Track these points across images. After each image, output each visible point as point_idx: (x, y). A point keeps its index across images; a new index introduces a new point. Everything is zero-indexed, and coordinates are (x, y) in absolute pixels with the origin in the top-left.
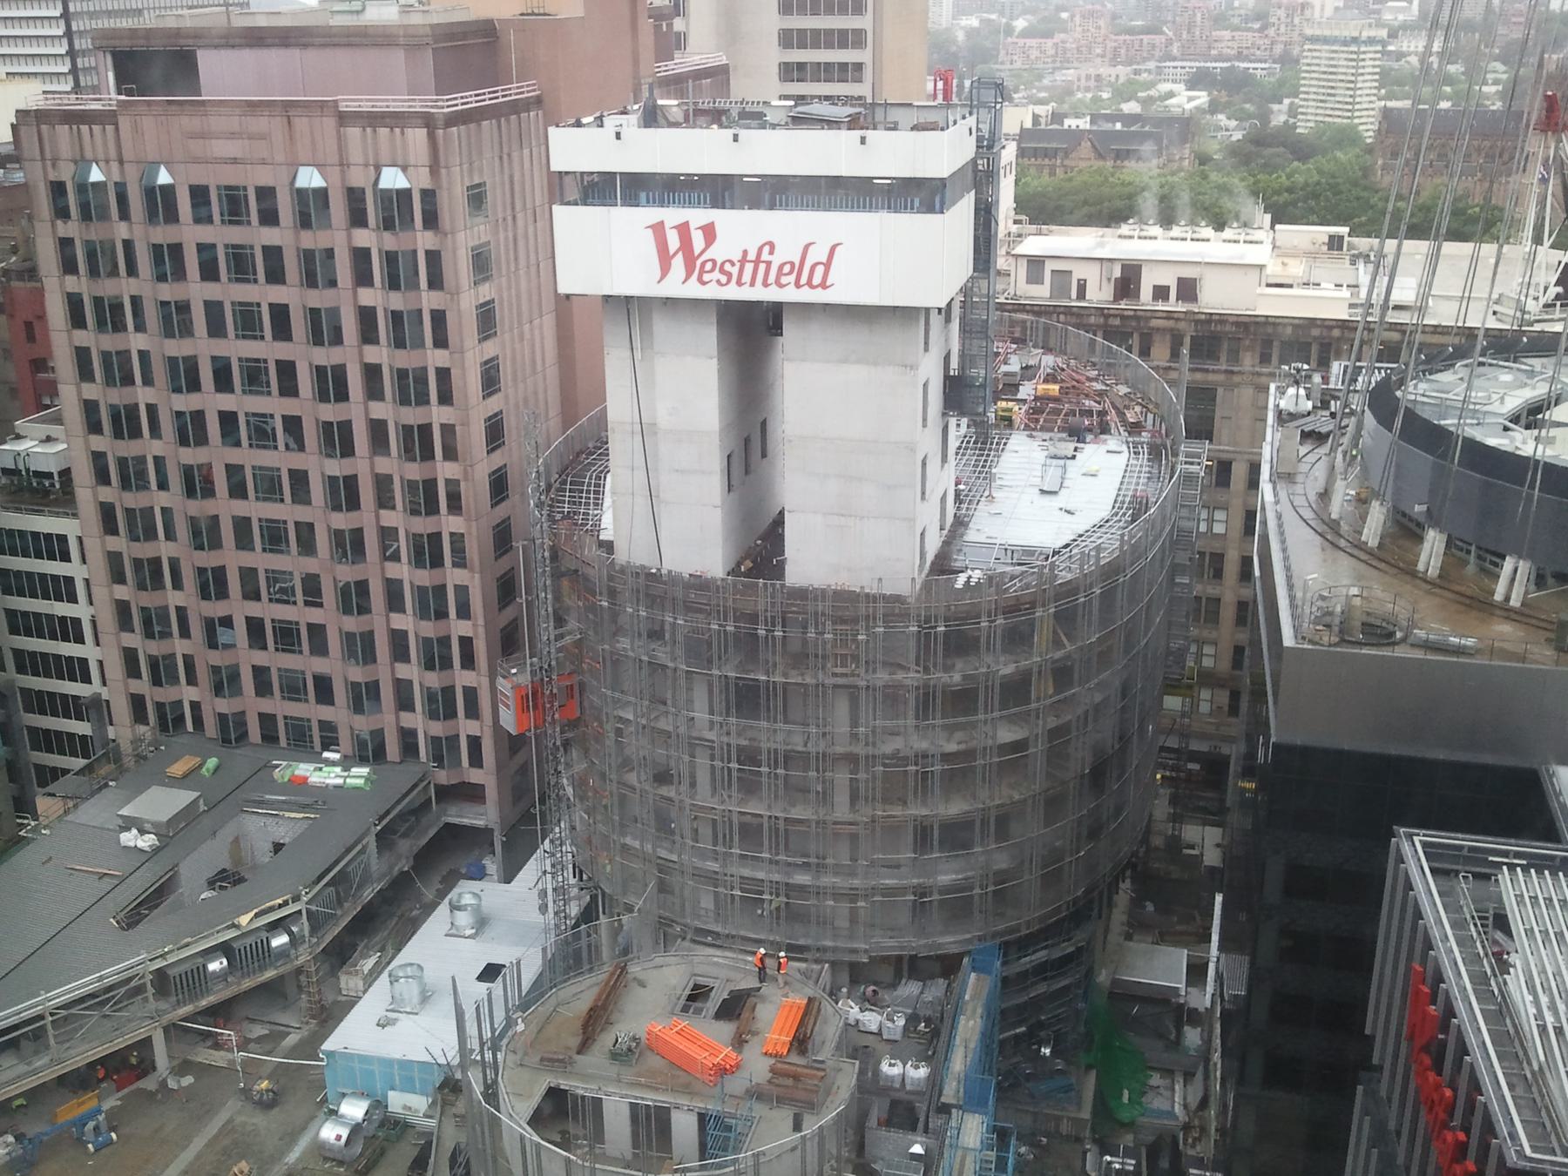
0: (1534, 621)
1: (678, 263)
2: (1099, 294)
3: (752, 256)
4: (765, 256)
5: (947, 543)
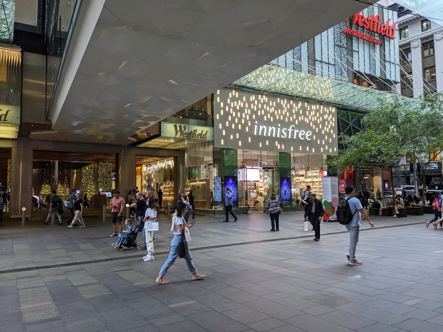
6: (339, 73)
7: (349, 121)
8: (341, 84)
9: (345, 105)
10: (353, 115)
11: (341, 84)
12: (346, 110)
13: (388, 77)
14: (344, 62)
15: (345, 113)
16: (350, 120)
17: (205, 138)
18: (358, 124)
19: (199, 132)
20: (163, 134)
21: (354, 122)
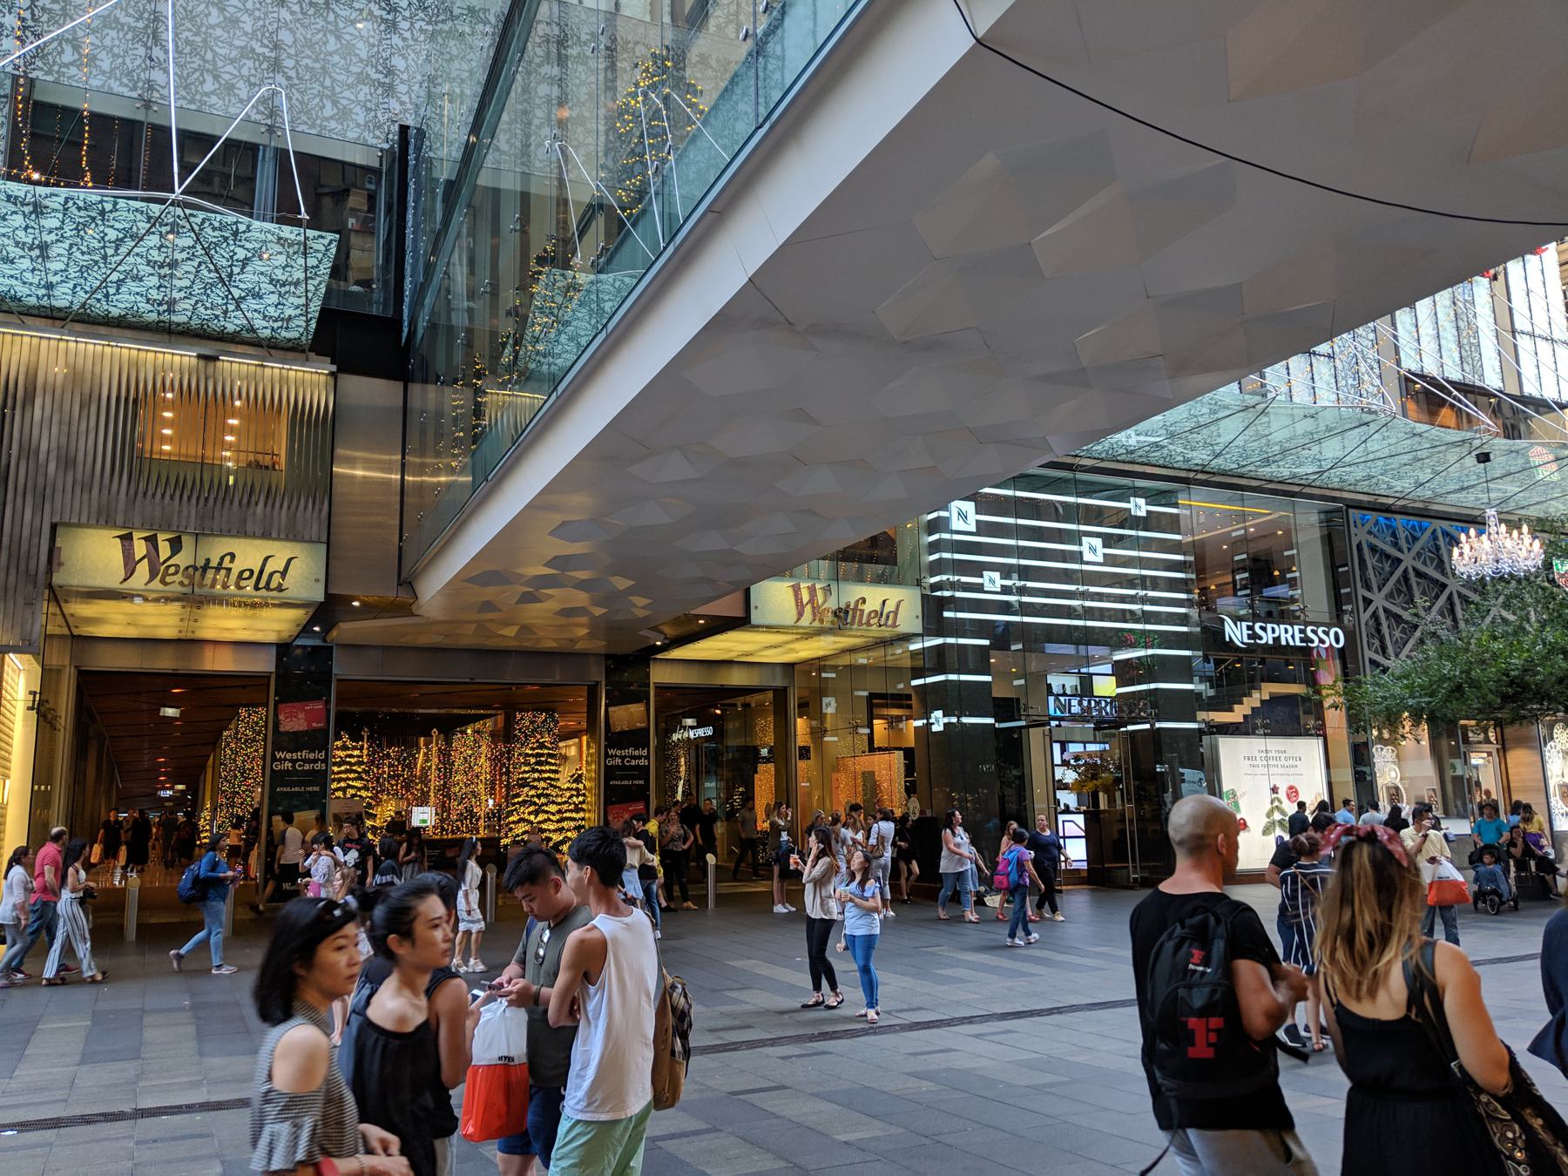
0: (1254, 483)
1: (143, 569)
2: (525, 719)
3: (214, 563)
4: (226, 563)
5: (469, 151)
6: (1350, 381)
7: (1400, 550)
8: (1367, 424)
9: (1336, 485)
10: (1413, 527)
11: (1367, 424)
12: (1387, 509)
13: (1530, 389)
14: (1366, 343)
15: (1382, 521)
16: (1404, 546)
17: (894, 625)
18: (1432, 560)
19: (872, 605)
20: (755, 618)
21: (1419, 554)
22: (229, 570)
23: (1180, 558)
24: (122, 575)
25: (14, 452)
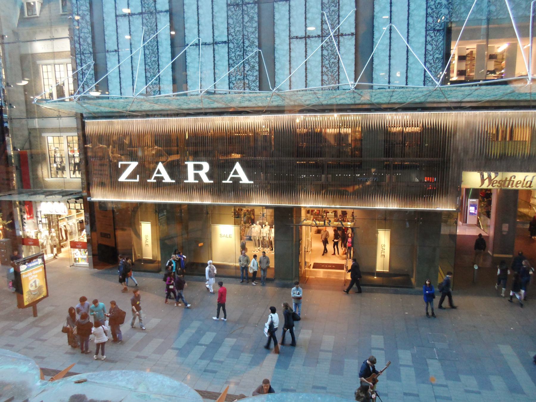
1: (486, 182)
3: (508, 179)
4: (513, 179)
22: (514, 181)
23: (273, 143)
24: (480, 184)
25: (452, 149)
